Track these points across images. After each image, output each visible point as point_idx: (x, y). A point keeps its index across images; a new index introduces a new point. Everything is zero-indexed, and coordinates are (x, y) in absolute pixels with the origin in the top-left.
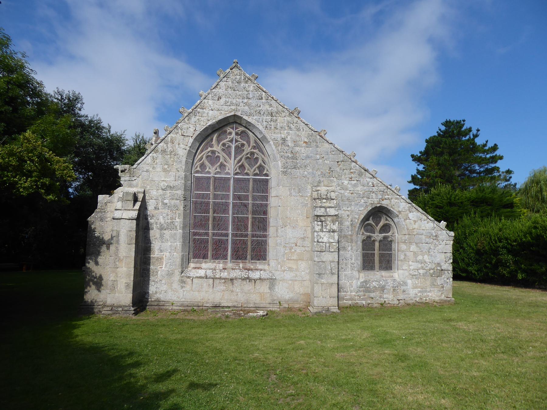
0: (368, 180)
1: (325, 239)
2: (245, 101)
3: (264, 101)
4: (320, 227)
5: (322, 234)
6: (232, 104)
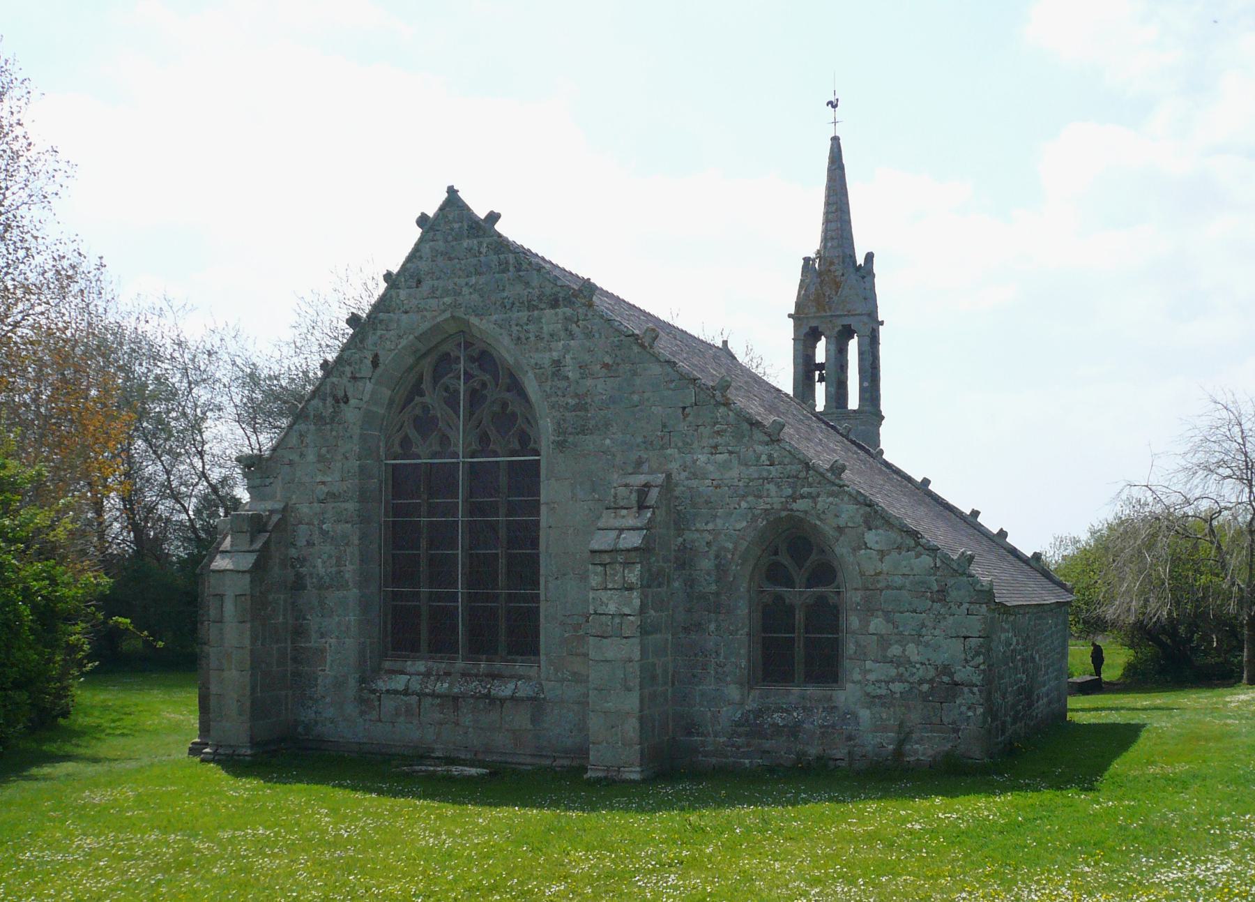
0: (759, 448)
1: (612, 608)
5: (604, 595)
6: (446, 292)
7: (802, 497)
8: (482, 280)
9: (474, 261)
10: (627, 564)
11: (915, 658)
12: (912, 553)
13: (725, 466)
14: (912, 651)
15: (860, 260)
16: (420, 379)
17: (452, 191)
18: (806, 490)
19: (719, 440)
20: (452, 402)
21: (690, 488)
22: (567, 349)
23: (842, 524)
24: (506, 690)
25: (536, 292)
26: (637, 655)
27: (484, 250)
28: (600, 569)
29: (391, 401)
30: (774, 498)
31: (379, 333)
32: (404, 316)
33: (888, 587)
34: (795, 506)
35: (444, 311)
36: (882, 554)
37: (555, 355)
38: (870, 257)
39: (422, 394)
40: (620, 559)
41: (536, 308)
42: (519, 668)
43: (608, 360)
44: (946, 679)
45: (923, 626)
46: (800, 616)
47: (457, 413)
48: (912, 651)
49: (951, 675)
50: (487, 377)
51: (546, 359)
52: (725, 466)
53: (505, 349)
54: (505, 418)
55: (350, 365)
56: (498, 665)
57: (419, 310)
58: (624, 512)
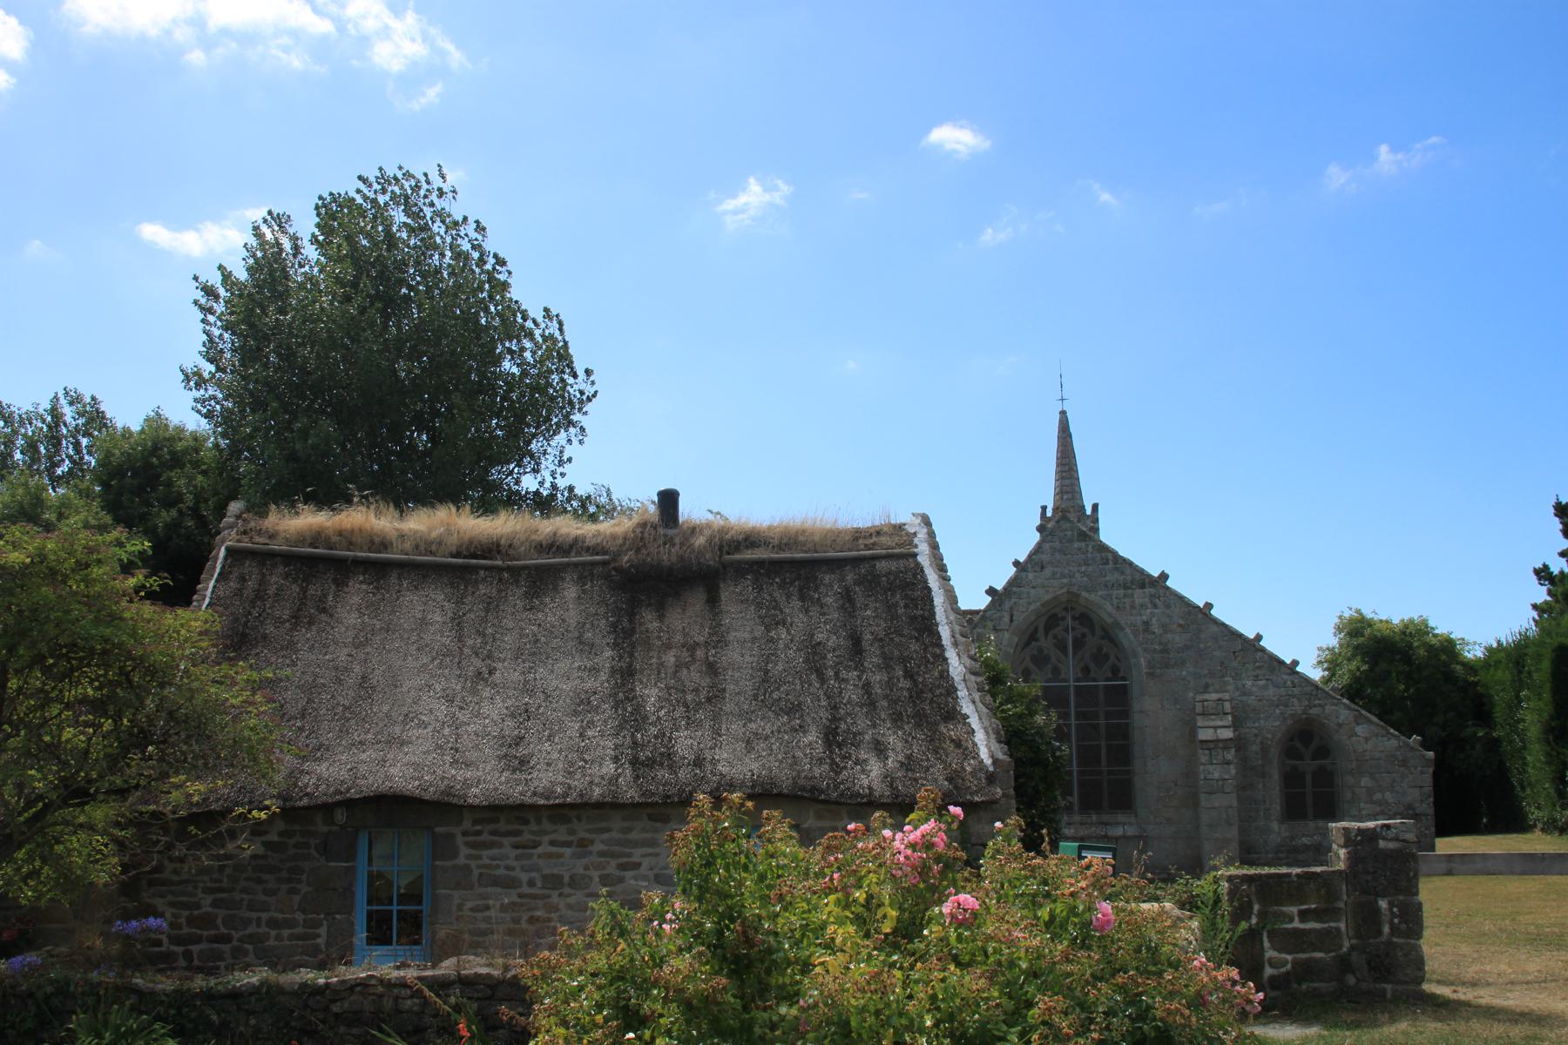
0: (1285, 677)
1: (1216, 775)
2: (1083, 569)
3: (1111, 565)
4: (1207, 758)
5: (1211, 768)
6: (1063, 576)
7: (1315, 706)
8: (1090, 569)
9: (1083, 557)
10: (1225, 748)
11: (1391, 801)
12: (1385, 739)
13: (1265, 688)
14: (1389, 796)
15: (1089, 511)
16: (1036, 630)
18: (1317, 702)
19: (1259, 672)
20: (1063, 648)
21: (1241, 701)
22: (1153, 614)
23: (1341, 721)
24: (1118, 831)
25: (1129, 578)
26: (1235, 804)
27: (1090, 549)
28: (1207, 752)
30: (1297, 707)
31: (1013, 600)
32: (1032, 591)
33: (1372, 759)
34: (1311, 712)
35: (1062, 588)
36: (1367, 739)
37: (1145, 618)
38: (1095, 507)
39: (1037, 640)
40: (1221, 745)
41: (1129, 588)
42: (1121, 818)
43: (1181, 622)
44: (1411, 812)
45: (1394, 781)
46: (1309, 778)
47: (1066, 654)
48: (1389, 796)
49: (1414, 809)
50: (1086, 630)
51: (1138, 620)
52: (1265, 688)
54: (1100, 658)
55: (992, 620)
56: (1106, 818)
57: (1043, 587)
58: (1213, 717)
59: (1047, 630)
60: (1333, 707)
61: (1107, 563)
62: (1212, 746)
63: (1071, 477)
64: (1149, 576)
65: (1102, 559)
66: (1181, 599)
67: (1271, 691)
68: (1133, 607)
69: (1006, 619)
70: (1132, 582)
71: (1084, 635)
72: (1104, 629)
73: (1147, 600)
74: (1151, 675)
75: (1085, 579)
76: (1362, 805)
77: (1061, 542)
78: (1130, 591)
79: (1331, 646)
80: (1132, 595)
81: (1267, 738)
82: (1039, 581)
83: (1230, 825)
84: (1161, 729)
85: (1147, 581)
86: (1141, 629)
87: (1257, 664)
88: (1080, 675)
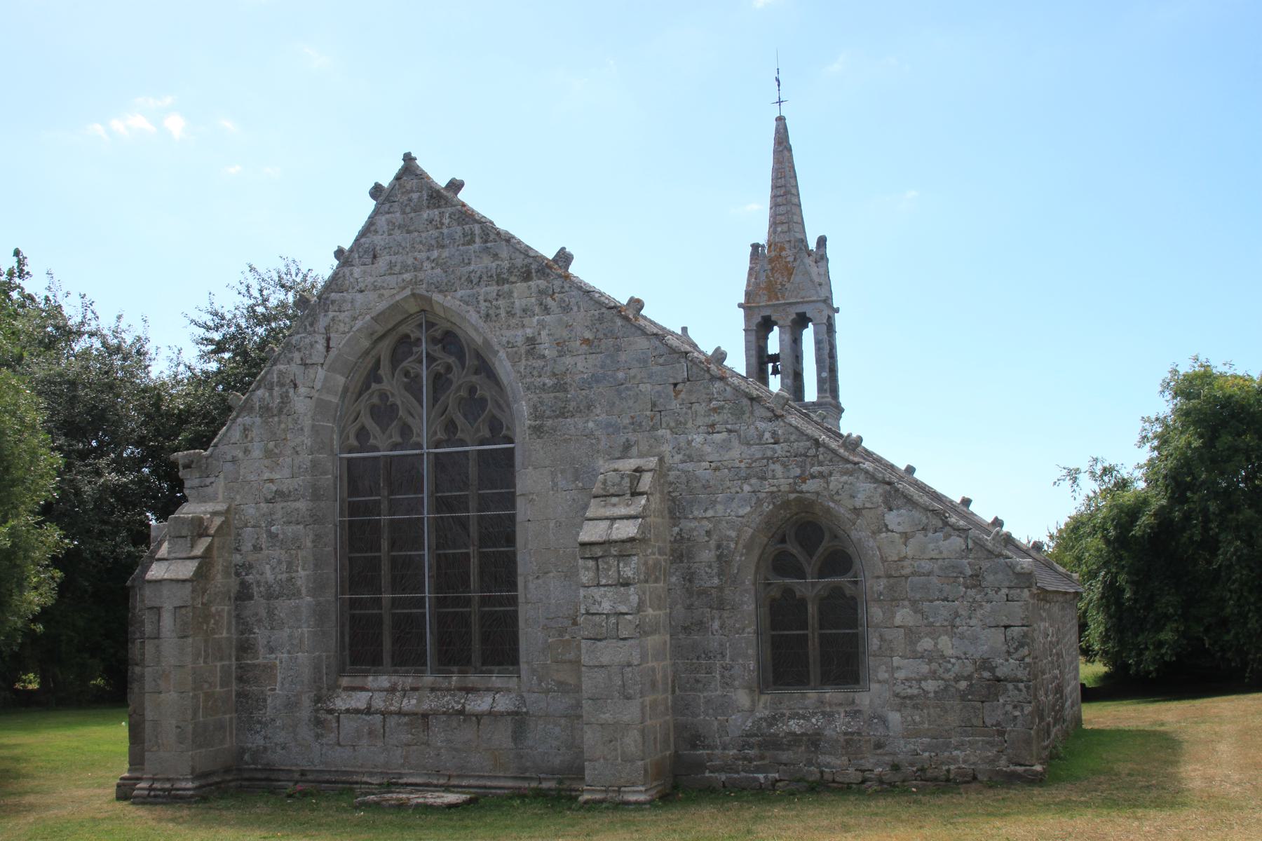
0: (762, 425)
1: (606, 607)
2: (435, 254)
3: (478, 245)
4: (591, 574)
5: (597, 593)
6: (405, 268)
7: (813, 477)
8: (446, 253)
9: (435, 233)
11: (949, 652)
13: (725, 446)
15: (812, 245)
17: (408, 158)
18: (816, 469)
19: (716, 418)
20: (413, 386)
21: (684, 471)
22: (542, 325)
23: (858, 504)
24: (481, 704)
25: (506, 264)
27: (446, 221)
28: (591, 563)
29: (346, 389)
30: (781, 479)
31: (331, 314)
32: (359, 296)
34: (804, 487)
35: (404, 288)
36: (906, 537)
37: (529, 332)
38: (822, 241)
39: (379, 380)
42: (496, 681)
43: (588, 335)
45: (957, 615)
46: (812, 609)
47: (422, 406)
49: (992, 670)
50: (451, 360)
51: (519, 336)
52: (725, 446)
53: (474, 326)
54: (473, 404)
55: (299, 350)
56: (473, 679)
57: (375, 288)
58: (615, 500)
59: (395, 361)
60: (845, 478)
61: (472, 242)
62: (598, 551)
63: (788, 203)
64: (538, 258)
65: (465, 235)
66: (588, 293)
67: (736, 452)
68: (510, 314)
69: (321, 347)
70: (510, 271)
71: (449, 368)
72: (478, 356)
73: (533, 300)
74: (537, 430)
75: (438, 271)
76: (896, 661)
77: (404, 213)
78: (506, 287)
79: (1161, 416)
80: (510, 293)
81: (729, 538)
82: (370, 279)
83: (628, 698)
84: (552, 525)
85: (534, 267)
86: (523, 350)
87: (714, 404)
88: (441, 435)
